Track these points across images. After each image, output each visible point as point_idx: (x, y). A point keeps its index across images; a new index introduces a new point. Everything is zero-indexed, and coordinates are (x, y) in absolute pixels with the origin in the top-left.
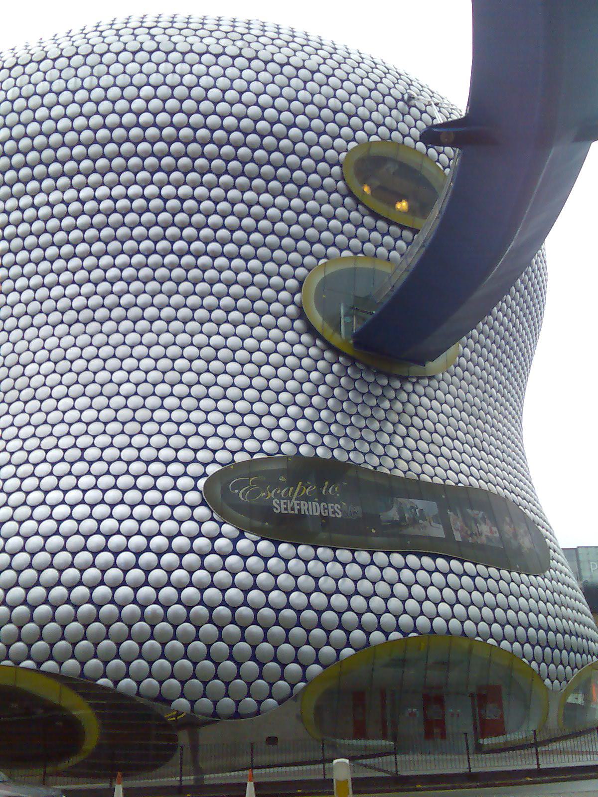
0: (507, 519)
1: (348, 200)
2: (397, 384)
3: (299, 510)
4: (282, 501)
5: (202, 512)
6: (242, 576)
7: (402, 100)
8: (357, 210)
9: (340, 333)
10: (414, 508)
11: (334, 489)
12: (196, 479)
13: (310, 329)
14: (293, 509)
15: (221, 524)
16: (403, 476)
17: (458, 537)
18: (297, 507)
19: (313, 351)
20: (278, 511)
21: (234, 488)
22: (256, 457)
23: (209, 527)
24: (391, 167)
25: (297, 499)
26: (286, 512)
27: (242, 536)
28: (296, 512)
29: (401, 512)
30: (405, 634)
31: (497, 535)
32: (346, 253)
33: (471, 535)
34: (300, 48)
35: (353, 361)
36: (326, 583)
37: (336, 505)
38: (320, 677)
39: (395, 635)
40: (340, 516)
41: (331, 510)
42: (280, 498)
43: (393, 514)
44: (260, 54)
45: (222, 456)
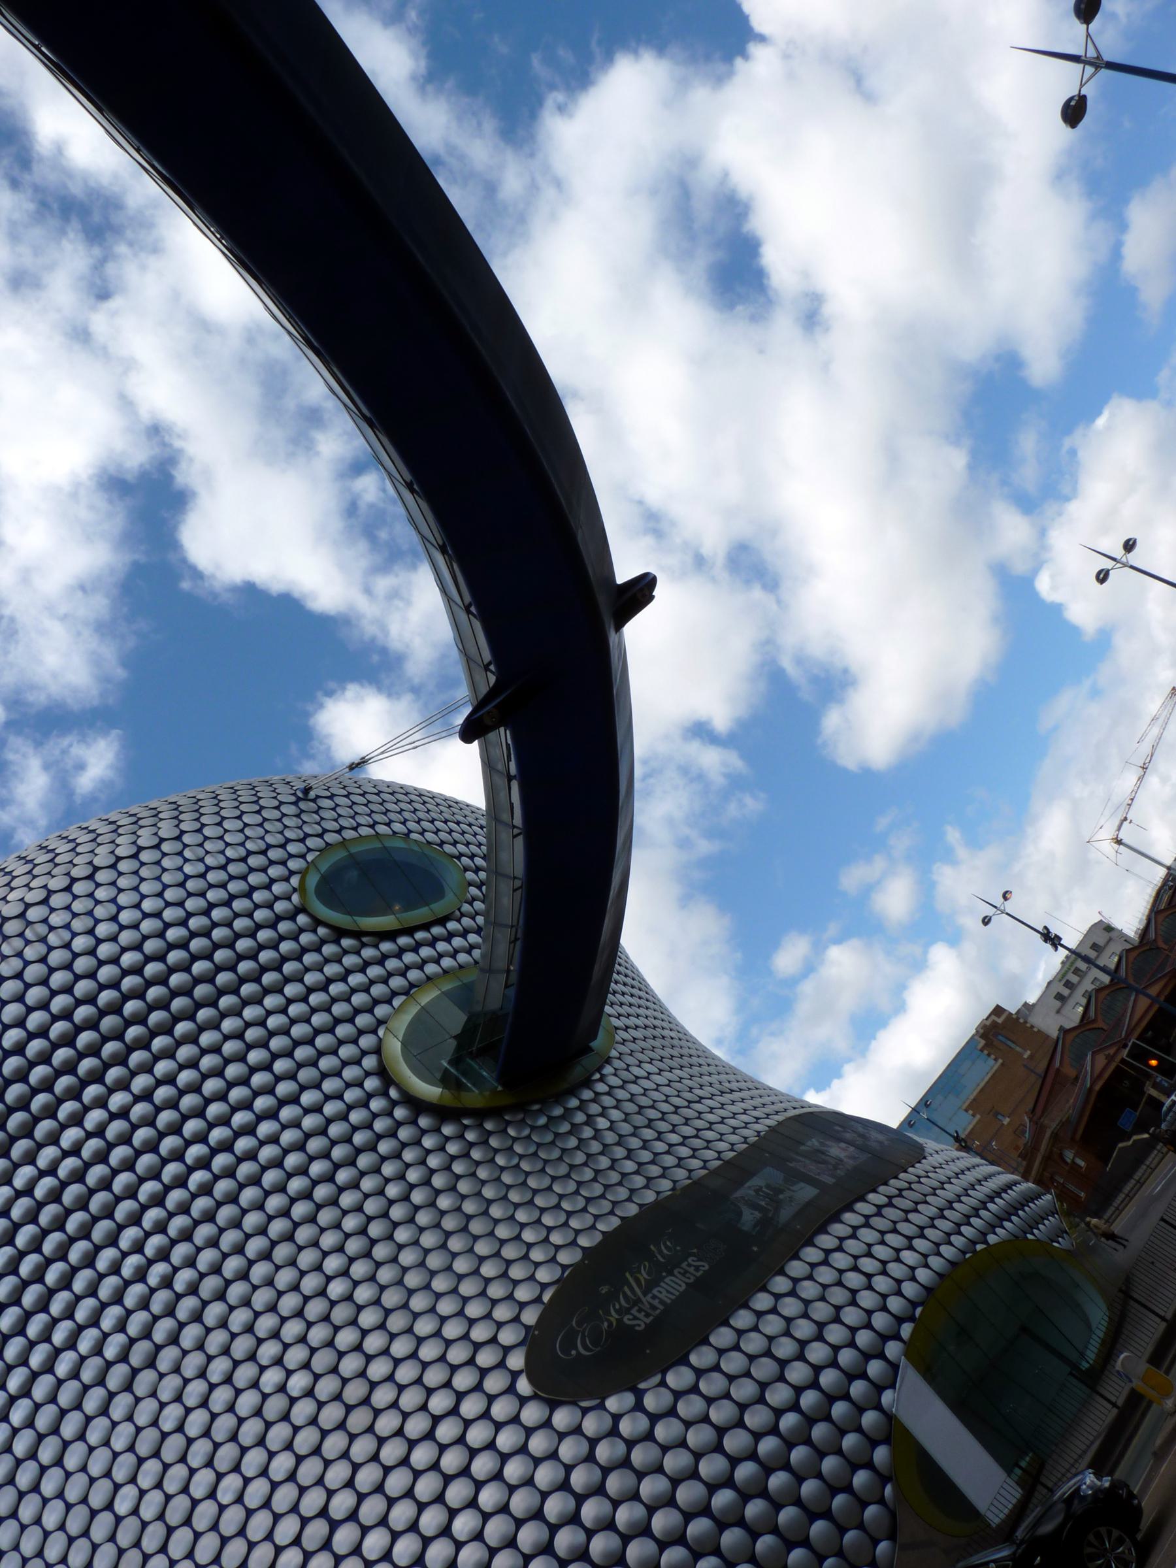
0: (837, 1128)
1: (346, 942)
2: (587, 1094)
3: (662, 1302)
4: (634, 1311)
5: (562, 1418)
6: (623, 1516)
7: (299, 799)
8: (364, 945)
9: (469, 1090)
10: (758, 1190)
11: (667, 1247)
12: (511, 1390)
13: (442, 1113)
14: (654, 1308)
15: (601, 1406)
16: (706, 1171)
17: (830, 1180)
18: (656, 1302)
19: (470, 1136)
20: (643, 1326)
21: (566, 1351)
22: (546, 1298)
23: (591, 1425)
24: (353, 874)
25: (645, 1294)
26: (651, 1318)
27: (639, 1395)
28: (662, 1307)
29: (755, 1206)
30: (911, 1319)
31: (852, 1149)
32: (396, 1002)
33: (835, 1168)
34: (29, 877)
35: (520, 1107)
36: (785, 1348)
37: (690, 1260)
38: (894, 1455)
39: (906, 1330)
40: (707, 1267)
41: (692, 1270)
42: (628, 1311)
43: (749, 1217)
44: (50, 887)
45: (508, 1336)
